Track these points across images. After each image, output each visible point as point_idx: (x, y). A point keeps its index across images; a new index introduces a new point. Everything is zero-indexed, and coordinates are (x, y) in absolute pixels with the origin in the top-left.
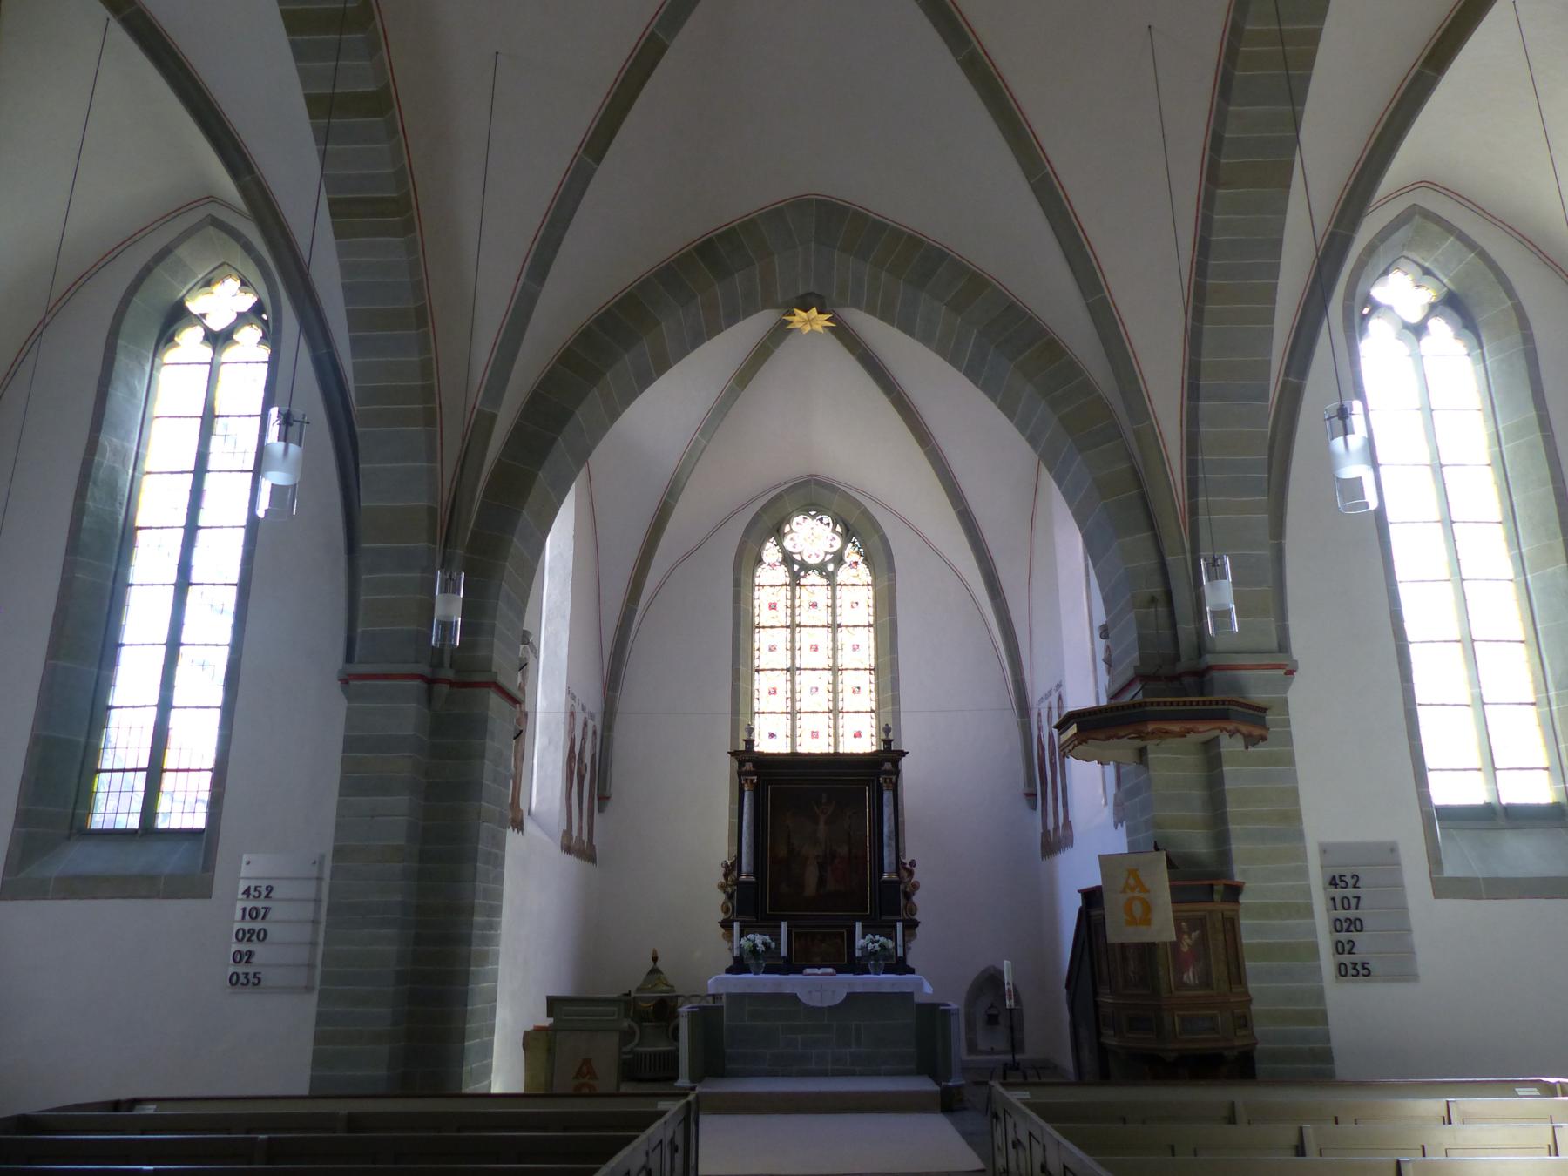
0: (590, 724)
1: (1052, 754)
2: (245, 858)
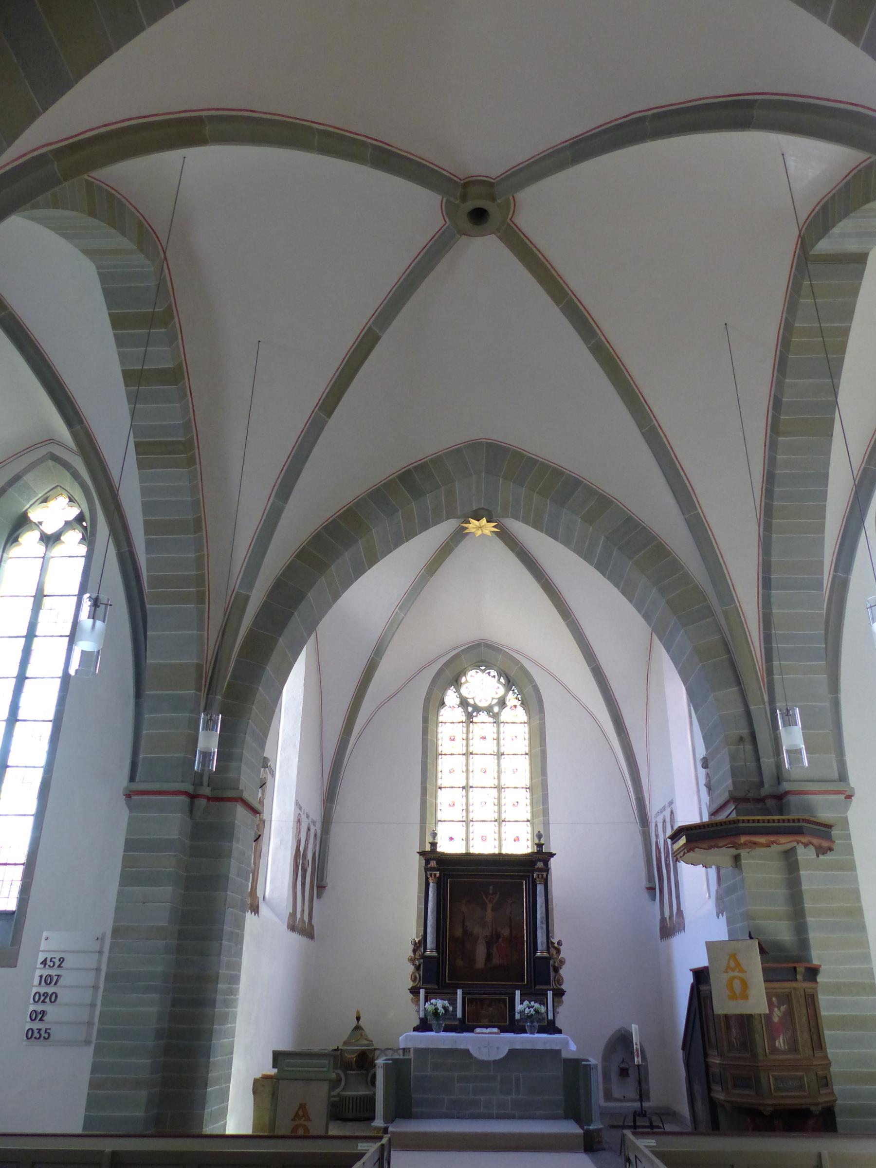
0: (313, 829)
1: (667, 857)
2: (45, 934)
